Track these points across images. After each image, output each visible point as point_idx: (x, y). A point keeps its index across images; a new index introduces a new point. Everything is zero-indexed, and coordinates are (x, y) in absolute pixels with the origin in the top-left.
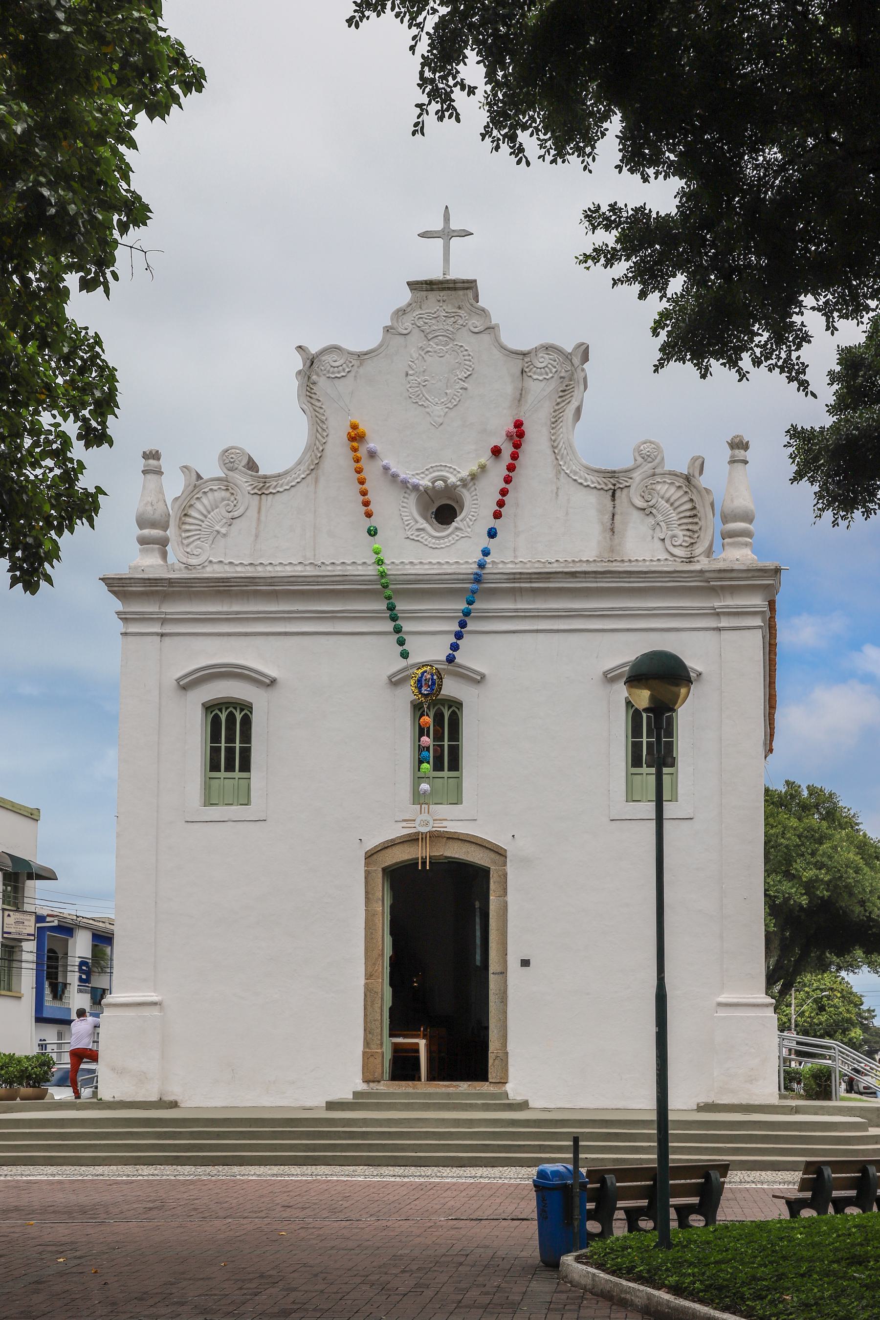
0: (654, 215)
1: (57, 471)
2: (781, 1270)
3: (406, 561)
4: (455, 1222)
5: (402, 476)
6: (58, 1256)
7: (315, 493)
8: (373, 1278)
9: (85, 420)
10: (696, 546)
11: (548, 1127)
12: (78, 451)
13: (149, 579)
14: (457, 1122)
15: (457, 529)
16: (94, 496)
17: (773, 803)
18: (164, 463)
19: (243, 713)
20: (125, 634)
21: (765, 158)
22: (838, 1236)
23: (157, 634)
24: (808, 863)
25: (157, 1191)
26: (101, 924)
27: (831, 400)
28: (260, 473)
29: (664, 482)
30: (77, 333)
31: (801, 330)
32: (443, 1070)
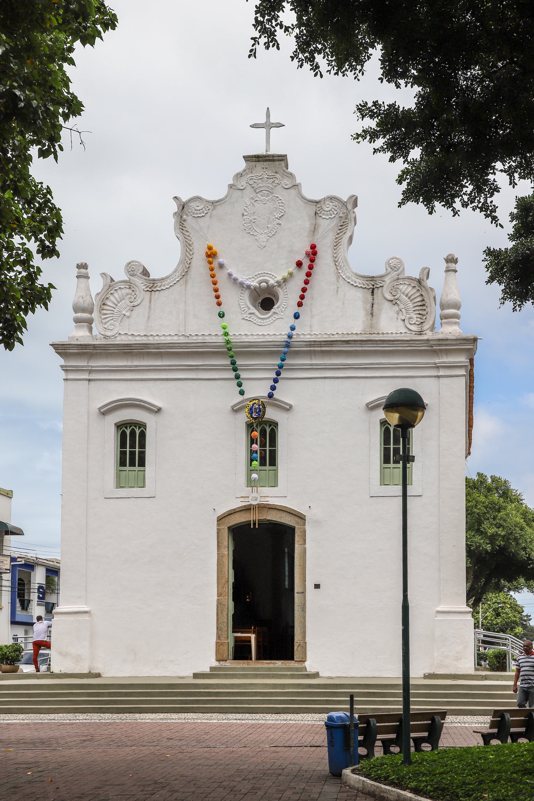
0: (401, 109)
1: (24, 274)
2: (481, 778)
3: (243, 334)
4: (275, 748)
5: (240, 280)
6: (28, 771)
7: (185, 290)
8: (225, 784)
9: (42, 241)
10: (424, 324)
11: (332, 689)
12: (37, 261)
13: (81, 345)
14: (275, 686)
15: (274, 313)
16: (48, 290)
17: (469, 487)
18: (90, 271)
19: (140, 430)
20: (66, 380)
21: (471, 73)
22: (516, 757)
23: (86, 380)
24: (491, 524)
25: (88, 730)
26: (51, 563)
27: (511, 231)
28: (151, 277)
29: (405, 283)
30: (36, 186)
31: (493, 184)
32: (268, 652)
